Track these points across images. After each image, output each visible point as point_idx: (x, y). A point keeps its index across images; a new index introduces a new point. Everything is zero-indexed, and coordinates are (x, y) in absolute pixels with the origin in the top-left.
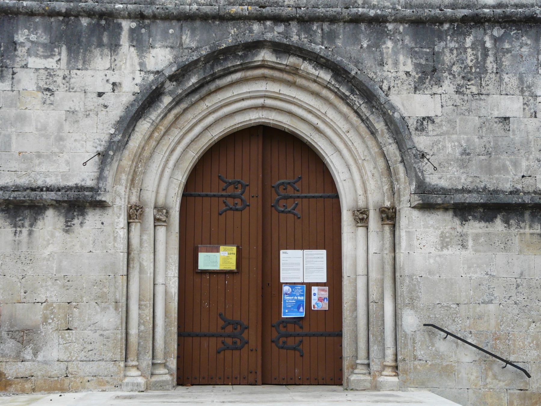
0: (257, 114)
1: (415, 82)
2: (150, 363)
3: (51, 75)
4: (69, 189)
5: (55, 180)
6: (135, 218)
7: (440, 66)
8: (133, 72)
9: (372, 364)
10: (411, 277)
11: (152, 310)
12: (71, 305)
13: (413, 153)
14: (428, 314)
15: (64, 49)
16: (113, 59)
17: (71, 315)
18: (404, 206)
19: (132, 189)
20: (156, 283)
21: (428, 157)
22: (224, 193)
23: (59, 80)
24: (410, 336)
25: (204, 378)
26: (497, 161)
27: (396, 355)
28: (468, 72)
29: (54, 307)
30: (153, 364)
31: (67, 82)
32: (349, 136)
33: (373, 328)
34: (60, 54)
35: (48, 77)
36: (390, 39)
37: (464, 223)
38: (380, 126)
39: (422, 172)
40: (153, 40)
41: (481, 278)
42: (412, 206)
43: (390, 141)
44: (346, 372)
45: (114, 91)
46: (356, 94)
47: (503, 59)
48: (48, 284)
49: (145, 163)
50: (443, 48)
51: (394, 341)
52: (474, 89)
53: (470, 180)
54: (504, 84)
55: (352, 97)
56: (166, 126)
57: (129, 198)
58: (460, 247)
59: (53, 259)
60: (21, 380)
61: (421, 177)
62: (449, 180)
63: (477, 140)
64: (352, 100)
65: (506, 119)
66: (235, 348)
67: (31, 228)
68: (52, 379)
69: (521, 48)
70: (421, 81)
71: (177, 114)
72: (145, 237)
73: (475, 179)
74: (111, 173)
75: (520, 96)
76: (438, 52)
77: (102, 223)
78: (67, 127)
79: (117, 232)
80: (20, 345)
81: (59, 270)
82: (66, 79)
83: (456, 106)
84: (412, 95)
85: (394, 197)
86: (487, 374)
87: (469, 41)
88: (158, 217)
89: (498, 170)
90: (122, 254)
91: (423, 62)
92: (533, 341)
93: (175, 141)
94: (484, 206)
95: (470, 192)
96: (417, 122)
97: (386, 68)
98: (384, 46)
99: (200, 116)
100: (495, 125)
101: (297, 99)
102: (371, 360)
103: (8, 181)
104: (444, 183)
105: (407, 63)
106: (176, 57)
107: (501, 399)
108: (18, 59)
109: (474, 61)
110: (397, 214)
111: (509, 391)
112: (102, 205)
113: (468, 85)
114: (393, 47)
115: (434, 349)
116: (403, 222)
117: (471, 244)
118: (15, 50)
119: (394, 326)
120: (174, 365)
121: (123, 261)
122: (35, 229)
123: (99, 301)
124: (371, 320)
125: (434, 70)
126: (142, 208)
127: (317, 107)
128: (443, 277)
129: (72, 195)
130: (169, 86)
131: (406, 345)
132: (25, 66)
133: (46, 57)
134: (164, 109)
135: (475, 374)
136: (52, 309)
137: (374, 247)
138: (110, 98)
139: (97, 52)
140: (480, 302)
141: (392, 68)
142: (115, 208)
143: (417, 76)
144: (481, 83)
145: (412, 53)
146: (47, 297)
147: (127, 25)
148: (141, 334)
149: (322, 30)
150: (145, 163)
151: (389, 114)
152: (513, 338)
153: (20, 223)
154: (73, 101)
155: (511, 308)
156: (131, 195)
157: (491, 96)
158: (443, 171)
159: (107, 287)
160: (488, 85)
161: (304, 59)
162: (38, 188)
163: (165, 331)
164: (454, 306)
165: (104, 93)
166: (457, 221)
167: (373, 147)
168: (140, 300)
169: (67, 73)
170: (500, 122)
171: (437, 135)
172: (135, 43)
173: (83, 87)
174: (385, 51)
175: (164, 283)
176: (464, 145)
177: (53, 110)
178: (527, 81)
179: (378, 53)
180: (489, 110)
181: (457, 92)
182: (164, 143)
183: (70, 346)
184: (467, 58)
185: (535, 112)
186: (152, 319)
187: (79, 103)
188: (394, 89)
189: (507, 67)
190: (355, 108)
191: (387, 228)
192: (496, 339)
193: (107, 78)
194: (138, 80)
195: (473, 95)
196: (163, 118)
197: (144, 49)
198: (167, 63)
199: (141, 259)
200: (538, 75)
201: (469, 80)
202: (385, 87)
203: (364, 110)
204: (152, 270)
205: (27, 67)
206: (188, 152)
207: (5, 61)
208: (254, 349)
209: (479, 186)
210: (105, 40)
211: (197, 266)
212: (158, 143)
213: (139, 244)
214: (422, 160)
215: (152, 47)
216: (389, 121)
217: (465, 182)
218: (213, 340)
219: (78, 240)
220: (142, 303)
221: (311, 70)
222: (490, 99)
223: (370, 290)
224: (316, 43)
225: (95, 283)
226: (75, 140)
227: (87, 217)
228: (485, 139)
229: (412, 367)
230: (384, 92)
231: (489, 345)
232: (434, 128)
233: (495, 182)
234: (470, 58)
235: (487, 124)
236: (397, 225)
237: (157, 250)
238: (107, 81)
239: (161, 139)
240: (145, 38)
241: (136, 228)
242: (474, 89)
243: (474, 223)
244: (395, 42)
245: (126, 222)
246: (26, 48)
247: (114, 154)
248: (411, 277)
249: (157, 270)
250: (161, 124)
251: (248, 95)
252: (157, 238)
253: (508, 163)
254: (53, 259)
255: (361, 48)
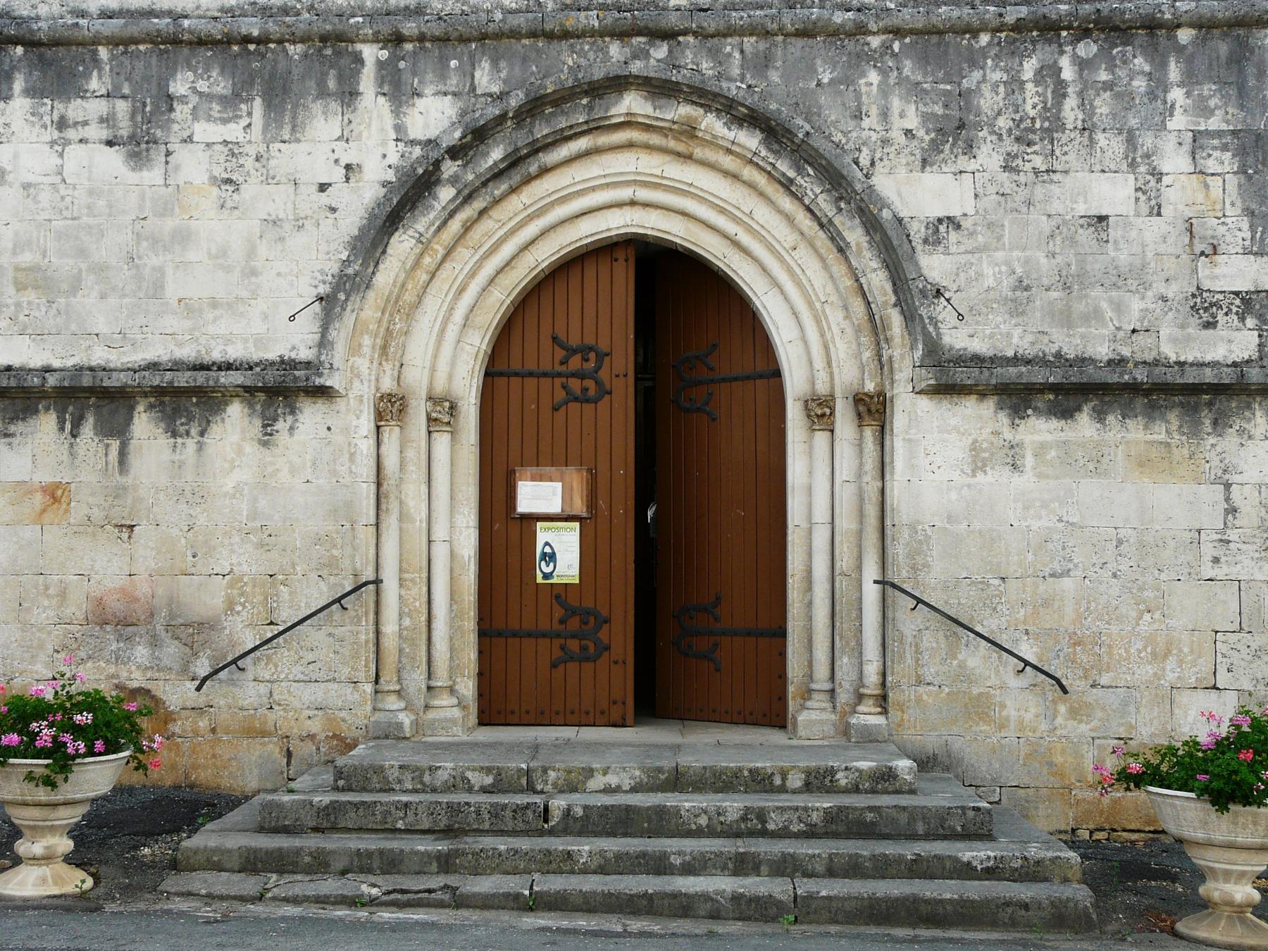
0: (622, 218)
1: (923, 149)
2: (424, 687)
3: (233, 155)
4: (267, 365)
5: (244, 349)
6: (389, 418)
7: (971, 117)
8: (384, 143)
9: (838, 690)
10: (913, 528)
11: (425, 589)
12: (275, 579)
13: (917, 287)
14: (946, 598)
15: (258, 102)
16: (346, 121)
17: (275, 598)
18: (901, 390)
19: (383, 363)
20: (433, 538)
21: (947, 295)
22: (563, 369)
23: (249, 163)
24: (910, 639)
25: (527, 712)
26: (1084, 303)
27: (884, 675)
28: (1026, 129)
29: (245, 583)
30: (429, 688)
31: (264, 167)
32: (796, 258)
33: (842, 623)
34: (250, 114)
35: (229, 158)
36: (875, 66)
37: (1017, 421)
38: (855, 235)
39: (936, 324)
40: (420, 82)
41: (1048, 528)
42: (917, 390)
43: (874, 264)
44: (792, 705)
45: (348, 180)
46: (809, 175)
47: (1096, 103)
48: (233, 541)
49: (408, 315)
50: (979, 82)
51: (880, 648)
52: (1038, 162)
53: (1030, 338)
54: (1099, 150)
55: (799, 180)
56: (446, 243)
57: (377, 380)
58: (1009, 467)
59: (241, 495)
60: (193, 714)
61: (934, 334)
62: (990, 339)
63: (1043, 261)
64: (801, 186)
65: (1102, 219)
66: (584, 657)
67: (201, 439)
68: (245, 713)
69: (1131, 79)
70: (936, 146)
71: (467, 221)
72: (410, 454)
73: (1041, 337)
74: (342, 335)
75: (1128, 173)
76: (969, 91)
77: (329, 429)
78: (263, 250)
79: (356, 444)
80: (188, 650)
81: (253, 515)
82: (262, 160)
83: (1003, 195)
84: (917, 175)
85: (882, 374)
86: (1055, 709)
87: (1029, 68)
88: (434, 415)
89: (1086, 319)
90: (365, 485)
91: (938, 109)
92: (1145, 648)
93: (465, 272)
94: (1056, 388)
95: (1028, 362)
96: (927, 228)
97: (866, 123)
98: (862, 81)
99: (512, 223)
100: (1081, 231)
101: (697, 187)
102: (837, 682)
103: (161, 352)
104: (979, 346)
105: (908, 114)
106: (463, 113)
107: (1082, 756)
108: (176, 127)
109: (1039, 107)
110: (888, 405)
111: (1097, 741)
112: (324, 392)
113: (1028, 154)
114: (880, 82)
115: (955, 662)
116: (899, 421)
117: (1031, 464)
118: (171, 109)
119: (880, 619)
120: (469, 690)
121: (368, 497)
122: (208, 441)
123: (324, 573)
124: (837, 608)
125: (962, 126)
126: (401, 399)
127: (734, 202)
128: (977, 525)
129: (271, 377)
130: (450, 168)
131: (902, 657)
132: (189, 140)
133: (225, 121)
134: (440, 211)
135: (1033, 710)
136: (243, 586)
137: (845, 469)
138: (340, 194)
139: (317, 107)
140: (1047, 574)
141: (878, 122)
142: (352, 401)
143: (927, 138)
144: (1053, 151)
145: (915, 91)
146: (231, 564)
147: (371, 53)
148: (405, 633)
149: (742, 52)
150: (408, 315)
151: (871, 212)
152: (1108, 642)
153: (182, 429)
154: (274, 200)
155: (1105, 585)
156: (382, 374)
157: (1072, 174)
158: (977, 323)
159: (339, 546)
160: (1066, 153)
161: (707, 108)
162: (214, 363)
163: (451, 627)
164: (997, 582)
165: (330, 185)
166: (1004, 418)
167: (842, 276)
168: (401, 570)
169: (262, 148)
170: (1089, 225)
171: (967, 252)
172: (386, 89)
173: (293, 174)
174: (864, 89)
175: (448, 539)
176: (1019, 270)
177: (240, 218)
178: (1143, 145)
179: (852, 95)
180: (1068, 202)
181: (1005, 167)
182: (444, 276)
183: (275, 653)
184: (1024, 101)
185: (1160, 207)
186: (425, 606)
187: (285, 204)
188: (882, 164)
189: (1104, 117)
190: (807, 202)
191: (869, 433)
192: (1075, 644)
193: (336, 156)
194: (394, 158)
195: (1036, 172)
196: (439, 229)
197: (404, 98)
198: (446, 124)
199: (403, 493)
200: (1166, 133)
201: (1028, 145)
202: (864, 160)
203: (823, 205)
204: (424, 515)
205: (192, 142)
206: (492, 292)
207: (152, 131)
208: (620, 661)
209: (1047, 351)
210: (332, 84)
211: (515, 508)
212: (433, 276)
213: (398, 465)
214: (936, 301)
215: (417, 95)
216: (872, 225)
217: (1020, 343)
218: (544, 643)
219: (285, 459)
220: (406, 576)
221: (721, 130)
222: (1068, 181)
223: (837, 552)
224: (730, 79)
225: (318, 541)
226: (279, 274)
227: (301, 417)
228: (1059, 259)
229: (913, 697)
230: (861, 170)
231: (1061, 654)
232: (961, 240)
233: (1079, 342)
234: (1031, 99)
235: (1065, 230)
236: (888, 427)
237: (434, 477)
238: (336, 161)
239: (437, 269)
240: (406, 77)
241: (391, 436)
242: (1038, 162)
243: (1037, 422)
244: (884, 73)
245: (372, 425)
246: (191, 106)
247: (347, 300)
248: (913, 528)
249: (434, 515)
250: (436, 240)
251: (603, 181)
252: (433, 456)
253: (1104, 305)
254: (241, 495)
255: (818, 85)
